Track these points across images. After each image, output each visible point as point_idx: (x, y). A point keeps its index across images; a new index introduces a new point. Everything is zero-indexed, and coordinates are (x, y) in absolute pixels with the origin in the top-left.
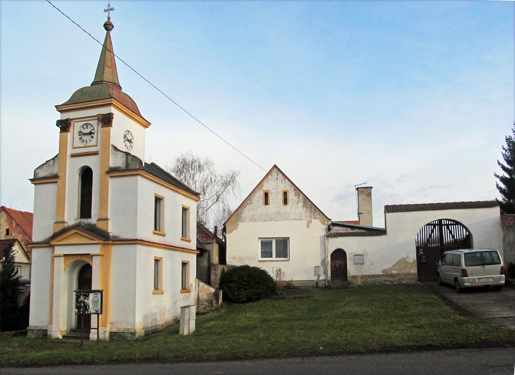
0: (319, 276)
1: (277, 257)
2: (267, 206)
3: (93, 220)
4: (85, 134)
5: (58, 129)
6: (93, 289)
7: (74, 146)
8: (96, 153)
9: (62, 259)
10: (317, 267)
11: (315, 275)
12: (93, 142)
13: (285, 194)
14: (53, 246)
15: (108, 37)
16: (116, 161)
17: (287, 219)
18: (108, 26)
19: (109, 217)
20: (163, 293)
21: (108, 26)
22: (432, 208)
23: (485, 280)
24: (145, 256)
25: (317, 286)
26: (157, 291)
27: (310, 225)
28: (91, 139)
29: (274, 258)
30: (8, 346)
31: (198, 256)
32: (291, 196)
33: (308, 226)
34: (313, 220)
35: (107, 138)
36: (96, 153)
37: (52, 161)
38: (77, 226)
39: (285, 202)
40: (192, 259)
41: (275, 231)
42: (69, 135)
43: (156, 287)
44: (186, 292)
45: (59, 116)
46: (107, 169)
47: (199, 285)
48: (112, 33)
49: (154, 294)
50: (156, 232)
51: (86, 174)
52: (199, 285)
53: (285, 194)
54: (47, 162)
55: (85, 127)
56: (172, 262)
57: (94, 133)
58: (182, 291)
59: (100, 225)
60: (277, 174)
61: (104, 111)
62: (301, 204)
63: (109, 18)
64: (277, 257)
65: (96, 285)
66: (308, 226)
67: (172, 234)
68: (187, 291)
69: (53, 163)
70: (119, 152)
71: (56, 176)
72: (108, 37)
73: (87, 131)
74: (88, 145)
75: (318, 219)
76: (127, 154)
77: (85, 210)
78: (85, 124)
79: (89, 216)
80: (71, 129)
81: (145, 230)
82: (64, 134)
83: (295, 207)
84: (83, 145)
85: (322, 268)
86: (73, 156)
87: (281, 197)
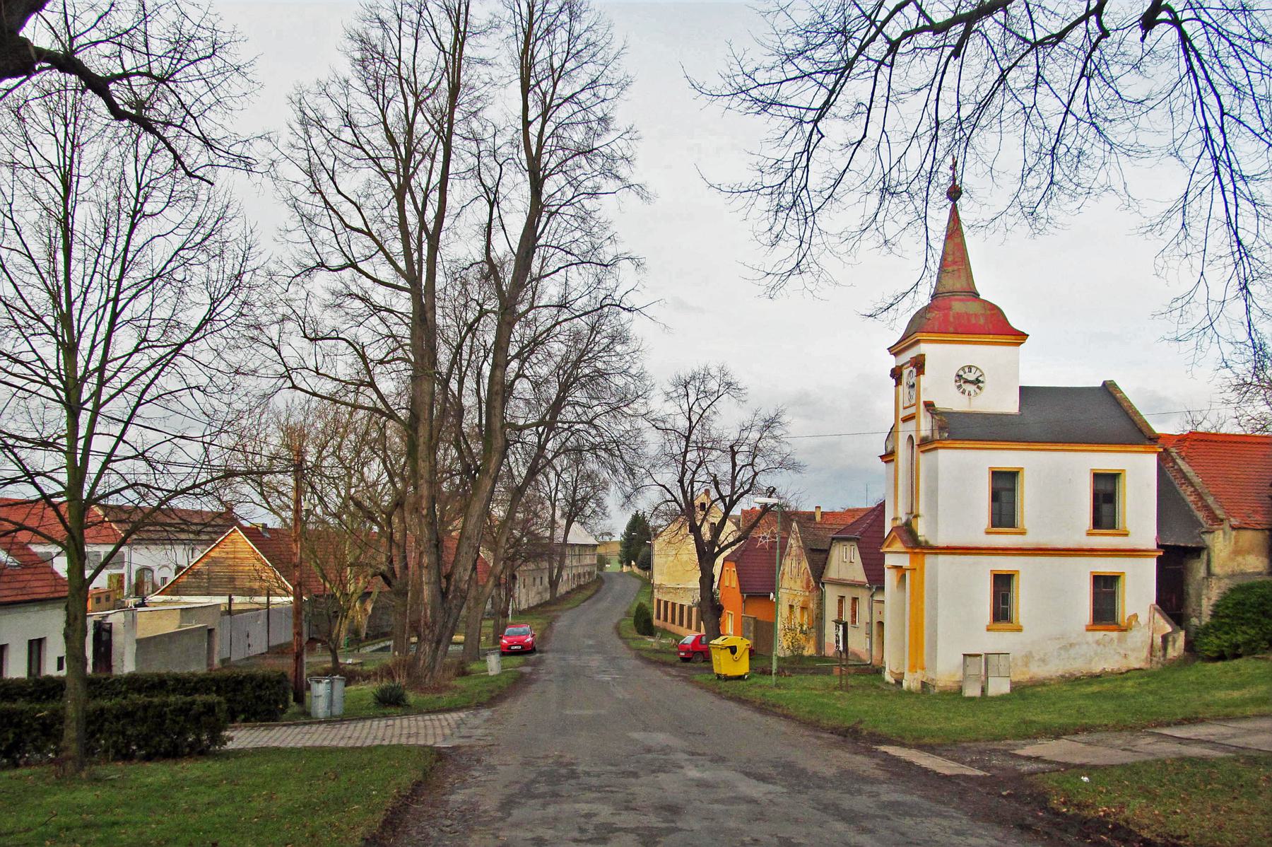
15: (954, 228)
29: (124, 571)
45: (892, 362)
73: (971, 377)
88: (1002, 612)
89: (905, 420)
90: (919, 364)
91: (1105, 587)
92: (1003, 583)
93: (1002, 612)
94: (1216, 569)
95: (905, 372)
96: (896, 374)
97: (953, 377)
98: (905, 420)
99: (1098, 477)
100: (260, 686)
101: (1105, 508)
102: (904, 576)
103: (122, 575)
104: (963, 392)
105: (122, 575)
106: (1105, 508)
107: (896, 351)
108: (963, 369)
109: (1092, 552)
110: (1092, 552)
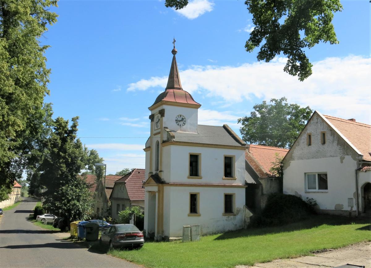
0: (352, 207)
1: (320, 188)
2: (310, 146)
4: (180, 121)
10: (350, 199)
11: (349, 206)
13: (324, 135)
15: (174, 59)
17: (325, 156)
18: (174, 52)
21: (174, 52)
22: (336, 136)
23: (116, 178)
25: (158, 187)
27: (344, 161)
29: (317, 190)
30: (20, 177)
32: (328, 137)
33: (342, 162)
34: (346, 157)
39: (324, 143)
41: (317, 166)
45: (150, 113)
53: (324, 135)
55: (179, 116)
60: (317, 119)
62: (336, 142)
64: (320, 188)
66: (342, 162)
71: (150, 147)
72: (174, 59)
73: (180, 119)
75: (350, 155)
83: (331, 147)
85: (354, 201)
87: (320, 137)
88: (194, 209)
89: (155, 134)
90: (162, 113)
91: (229, 200)
92: (194, 198)
93: (194, 209)
94: (265, 192)
95: (156, 117)
96: (152, 117)
97: (177, 115)
98: (155, 134)
99: (226, 158)
100: (271, 143)
101: (228, 170)
102: (155, 196)
103: (316, 189)
104: (178, 125)
105: (316, 189)
106: (228, 170)
107: (151, 109)
108: (178, 116)
109: (225, 186)
110: (225, 186)
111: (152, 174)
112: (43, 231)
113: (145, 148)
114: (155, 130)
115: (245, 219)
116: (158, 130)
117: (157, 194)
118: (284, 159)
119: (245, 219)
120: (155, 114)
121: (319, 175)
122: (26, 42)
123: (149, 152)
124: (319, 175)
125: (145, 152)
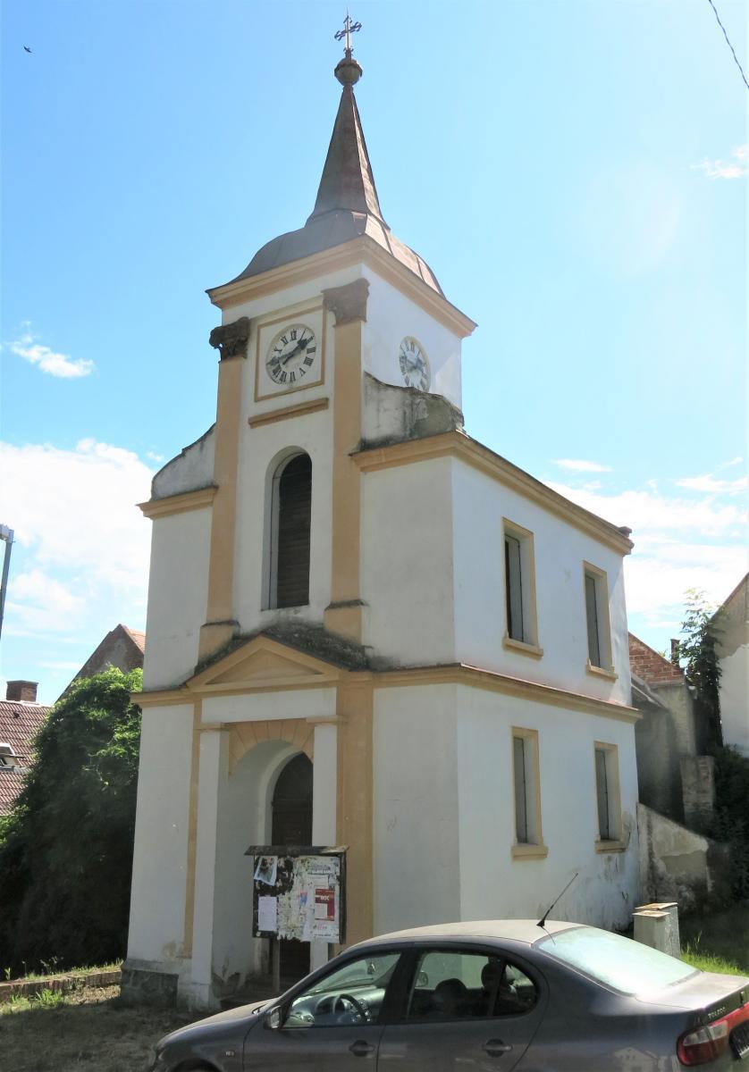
3: (313, 612)
5: (217, 354)
6: (261, 898)
7: (262, 393)
8: (321, 404)
9: (216, 736)
12: (312, 374)
14: (197, 700)
15: (348, 101)
16: (382, 420)
18: (348, 72)
19: (364, 595)
20: (543, 855)
21: (348, 72)
24: (476, 731)
26: (526, 849)
28: (305, 367)
31: (641, 729)
35: (350, 355)
36: (321, 404)
37: (199, 444)
38: (269, 632)
40: (624, 739)
42: (248, 365)
43: (524, 836)
44: (613, 850)
45: (215, 318)
46: (353, 446)
47: (650, 827)
48: (358, 89)
49: (515, 857)
50: (598, 555)
51: (294, 477)
52: (650, 827)
54: (185, 450)
56: (567, 748)
57: (313, 350)
58: (602, 846)
59: (339, 625)
61: (339, 278)
63: (348, 52)
65: (324, 830)
67: (560, 660)
68: (616, 845)
69: (202, 448)
70: (390, 391)
71: (213, 487)
72: (348, 101)
74: (296, 384)
76: (411, 391)
77: (290, 577)
78: (284, 331)
79: (304, 600)
80: (252, 349)
81: (478, 635)
82: (232, 364)
84: (284, 387)
86: (256, 422)
111: (415, 380)
112: (371, 766)
113: (147, 497)
114: (257, 400)
115: (652, 867)
116: (214, 690)
117: (86, 986)
118: (213, 959)
119: (652, 867)
120: (255, 319)
121: (316, 894)
122: (160, 1025)
123: (200, 521)
124: (316, 894)
125: (149, 522)
